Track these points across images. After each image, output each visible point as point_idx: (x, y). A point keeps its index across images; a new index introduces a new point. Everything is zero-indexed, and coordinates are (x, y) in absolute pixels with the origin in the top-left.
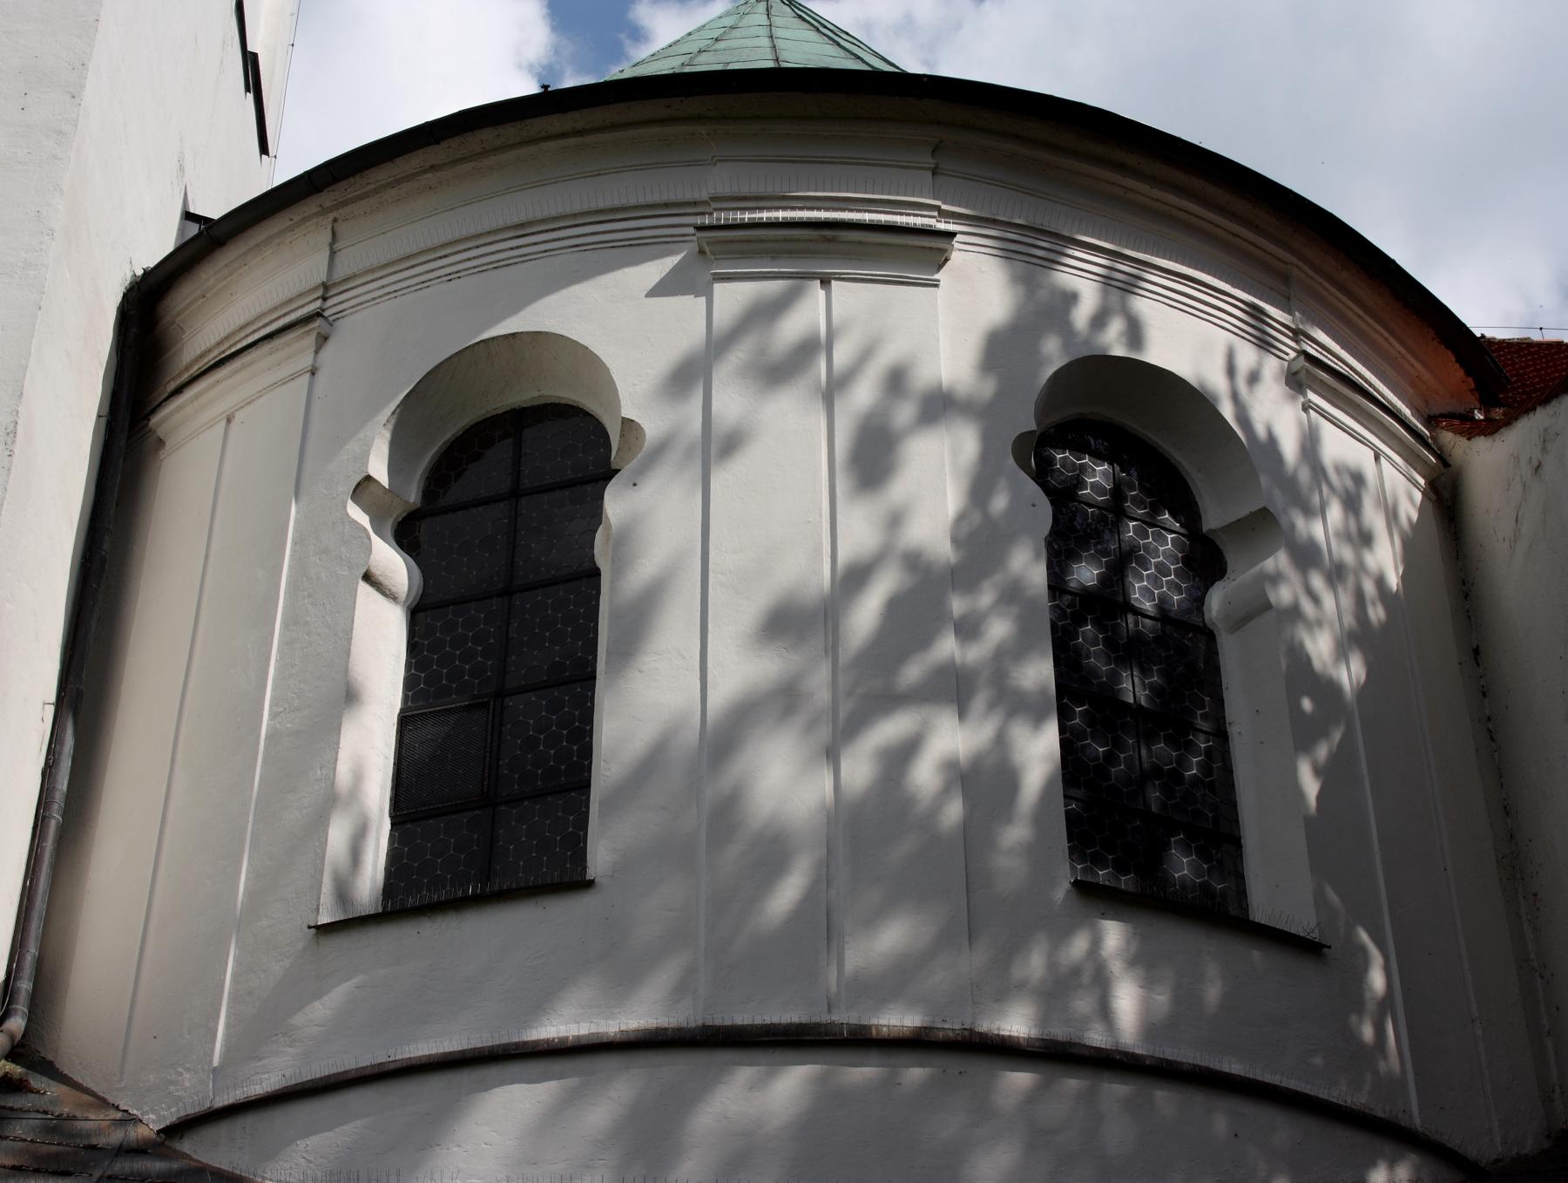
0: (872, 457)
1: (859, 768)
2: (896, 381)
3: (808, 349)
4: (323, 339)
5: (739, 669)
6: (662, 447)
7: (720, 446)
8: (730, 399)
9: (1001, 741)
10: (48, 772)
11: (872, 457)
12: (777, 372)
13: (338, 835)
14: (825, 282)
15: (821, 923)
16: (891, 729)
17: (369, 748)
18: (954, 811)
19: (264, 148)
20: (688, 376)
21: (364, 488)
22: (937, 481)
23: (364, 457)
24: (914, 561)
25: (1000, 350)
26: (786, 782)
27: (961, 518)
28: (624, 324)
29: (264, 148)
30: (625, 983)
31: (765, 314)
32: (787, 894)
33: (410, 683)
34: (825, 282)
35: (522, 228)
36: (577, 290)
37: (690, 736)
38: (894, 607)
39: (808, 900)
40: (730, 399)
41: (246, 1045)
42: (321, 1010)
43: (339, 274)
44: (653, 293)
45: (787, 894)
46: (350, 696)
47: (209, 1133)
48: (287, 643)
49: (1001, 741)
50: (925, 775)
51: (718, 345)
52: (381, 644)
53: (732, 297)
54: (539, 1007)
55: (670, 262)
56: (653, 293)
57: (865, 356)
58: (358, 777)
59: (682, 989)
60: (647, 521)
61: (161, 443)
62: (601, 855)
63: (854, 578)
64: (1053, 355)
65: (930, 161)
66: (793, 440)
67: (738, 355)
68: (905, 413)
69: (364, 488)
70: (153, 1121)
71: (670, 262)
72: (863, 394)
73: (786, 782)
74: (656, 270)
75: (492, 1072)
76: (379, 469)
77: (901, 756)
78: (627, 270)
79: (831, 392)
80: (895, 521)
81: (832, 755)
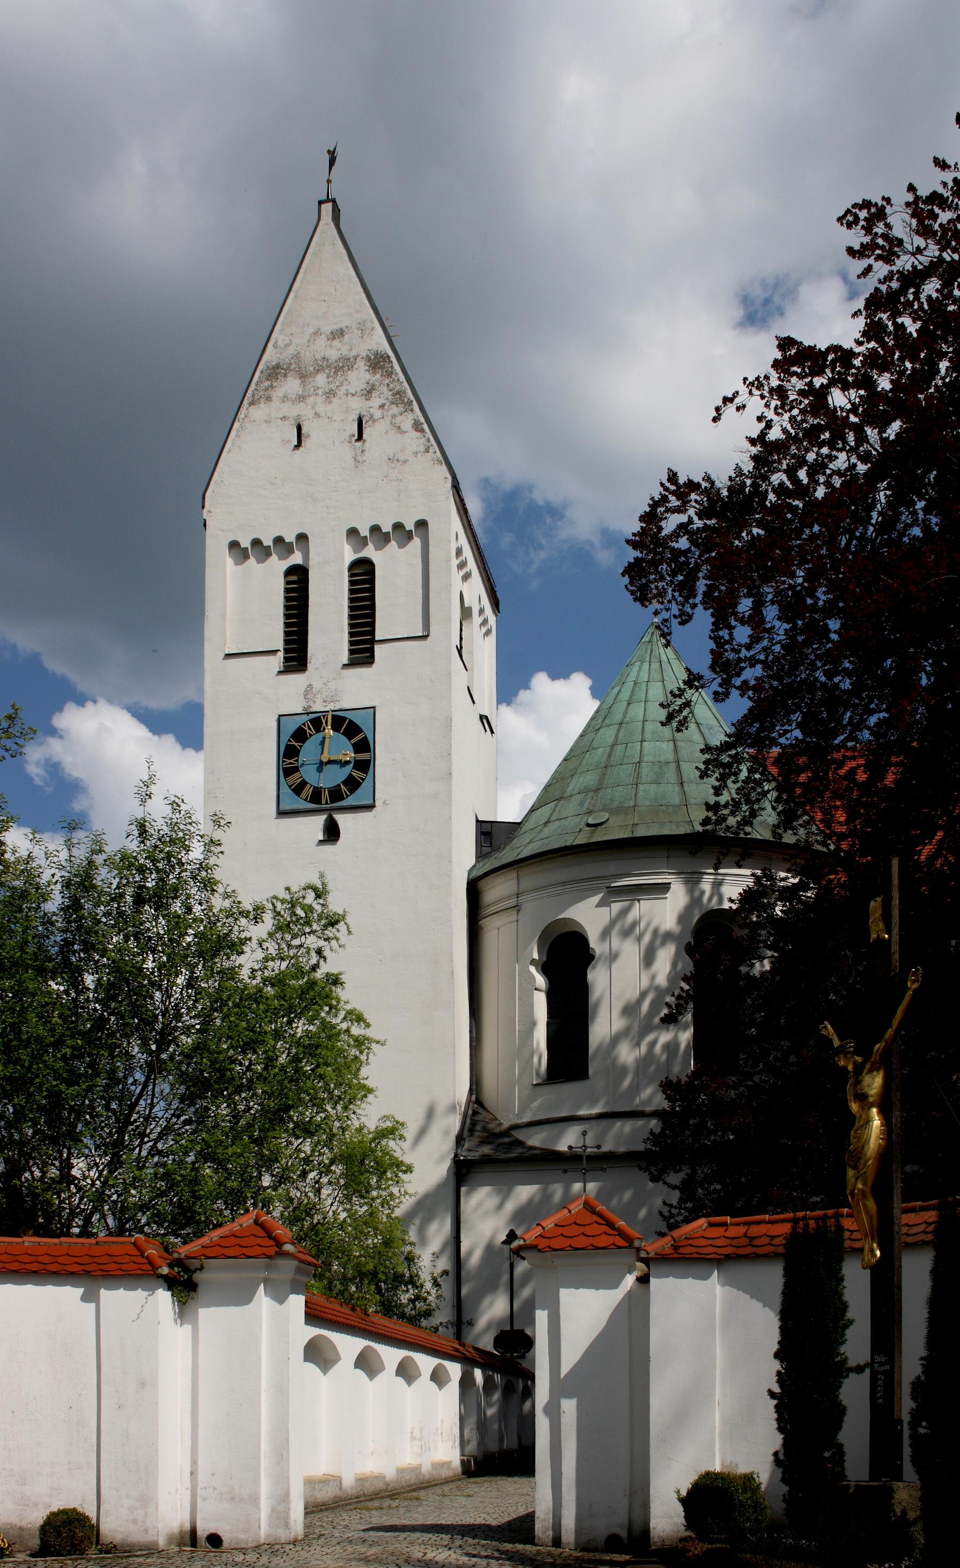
0: (649, 959)
1: (644, 1048)
2: (655, 932)
3: (635, 924)
4: (519, 911)
5: (618, 1024)
6: (599, 958)
7: (613, 957)
8: (616, 942)
9: (676, 1037)
10: (471, 1032)
11: (649, 959)
12: (626, 933)
13: (535, 1060)
14: (639, 900)
15: (635, 1089)
16: (650, 1038)
17: (540, 1035)
18: (664, 1057)
19: (474, 702)
20: (606, 934)
21: (533, 962)
22: (665, 958)
23: (532, 953)
24: (658, 989)
25: (682, 919)
26: (627, 1054)
27: (670, 973)
28: (589, 915)
29: (474, 702)
30: (594, 1102)
31: (624, 912)
32: (626, 1083)
33: (549, 1013)
34: (639, 900)
35: (564, 883)
36: (573, 907)
37: (608, 1039)
38: (652, 1003)
39: (631, 1084)
40: (616, 942)
41: (523, 1109)
42: (536, 1104)
43: (521, 890)
44: (597, 906)
45: (626, 1083)
46: (534, 1024)
47: (519, 1131)
48: (520, 1005)
49: (676, 1037)
50: (658, 1048)
51: (613, 923)
52: (540, 1003)
53: (616, 907)
54: (579, 1108)
55: (601, 895)
56: (597, 906)
57: (648, 925)
58: (538, 1044)
59: (606, 1105)
60: (597, 977)
61: (482, 928)
62: (591, 1071)
63: (643, 995)
64: (696, 916)
65: (666, 854)
66: (630, 952)
67: (617, 928)
68: (658, 942)
69: (533, 962)
70: (506, 1124)
71: (601, 895)
72: (647, 938)
73: (627, 1054)
74: (596, 899)
75: (571, 1123)
76: (536, 956)
77: (653, 1044)
78: (583, 1292)
79: (639, 939)
80: (653, 978)
81: (638, 1044)
